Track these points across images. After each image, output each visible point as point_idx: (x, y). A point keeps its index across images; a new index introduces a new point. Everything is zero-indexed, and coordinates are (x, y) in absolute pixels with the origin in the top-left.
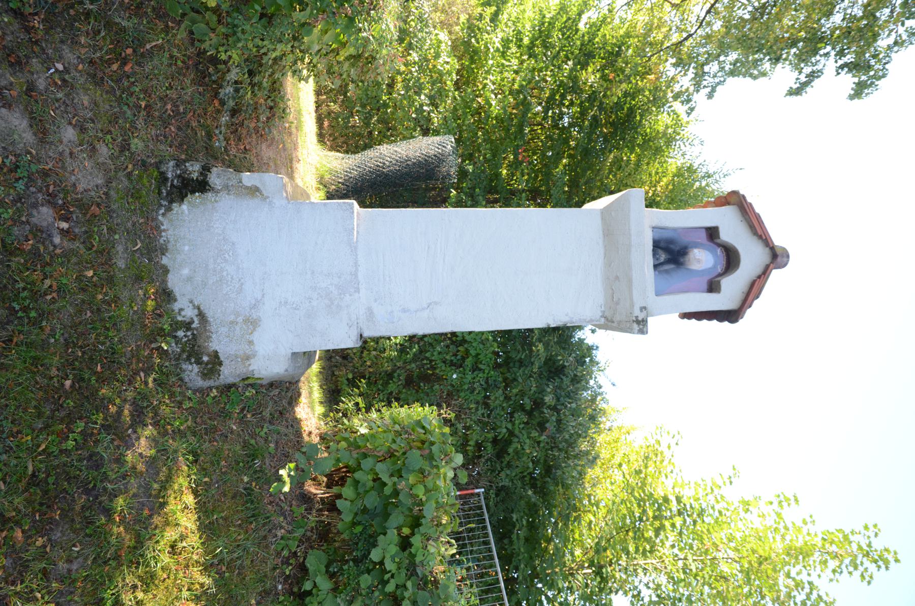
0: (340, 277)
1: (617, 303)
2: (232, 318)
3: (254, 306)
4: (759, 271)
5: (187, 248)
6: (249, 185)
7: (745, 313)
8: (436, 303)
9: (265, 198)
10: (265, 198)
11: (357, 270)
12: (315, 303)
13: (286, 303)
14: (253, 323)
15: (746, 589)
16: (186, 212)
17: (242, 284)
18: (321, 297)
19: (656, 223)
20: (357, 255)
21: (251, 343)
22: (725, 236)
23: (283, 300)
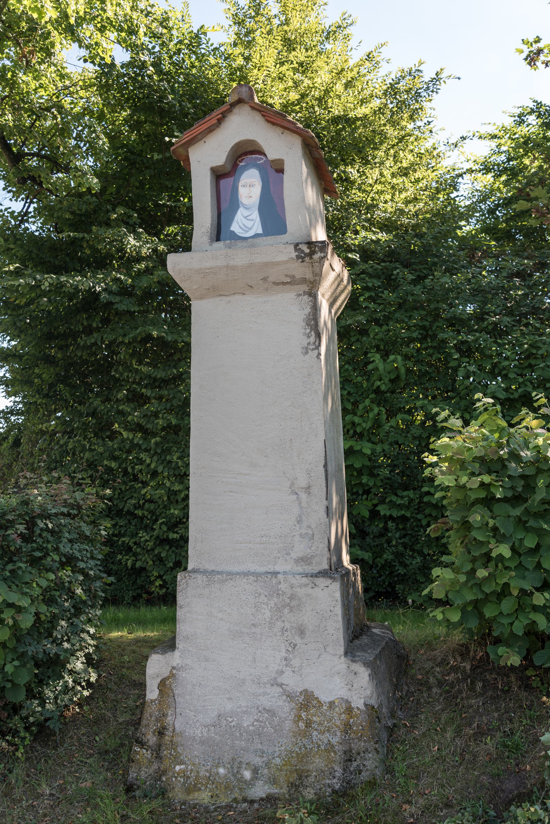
0: (260, 594)
1: (293, 277)
2: (302, 725)
3: (290, 697)
4: (258, 117)
5: (222, 771)
6: (157, 692)
7: (196, 145)
8: (292, 484)
9: (172, 675)
10: (172, 675)
11: (253, 574)
12: (287, 625)
13: (286, 659)
14: (307, 701)
15: (144, 596)
16: (183, 767)
17: (264, 709)
18: (281, 617)
19: (206, 239)
20: (238, 574)
21: (332, 704)
22: (220, 158)
23: (285, 663)
